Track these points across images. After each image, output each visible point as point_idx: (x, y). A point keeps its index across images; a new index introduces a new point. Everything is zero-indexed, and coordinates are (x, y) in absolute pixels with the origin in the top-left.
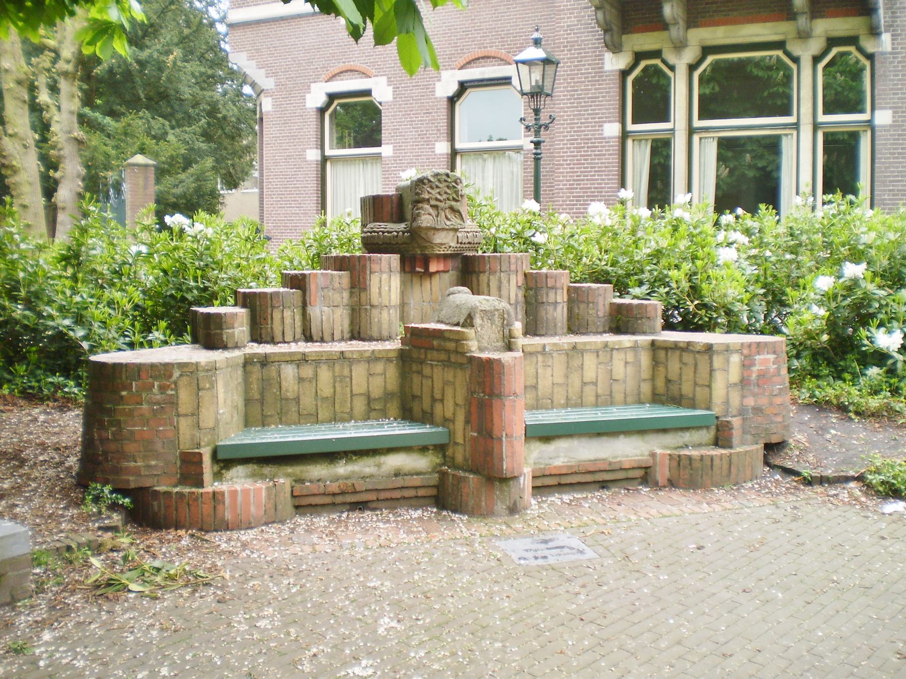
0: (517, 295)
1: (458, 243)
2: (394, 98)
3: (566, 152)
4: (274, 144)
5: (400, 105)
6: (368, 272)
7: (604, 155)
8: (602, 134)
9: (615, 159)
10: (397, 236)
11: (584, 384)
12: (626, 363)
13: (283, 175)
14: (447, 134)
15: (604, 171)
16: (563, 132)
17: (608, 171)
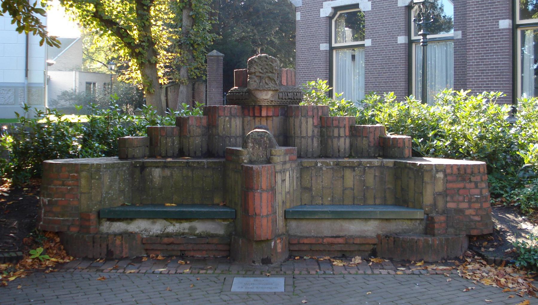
0: (313, 131)
1: (279, 98)
2: (372, 9)
3: (474, 40)
4: (302, 41)
5: (375, 13)
6: (217, 117)
7: (499, 41)
8: (498, 27)
9: (508, 45)
10: (242, 95)
11: (344, 189)
12: (375, 176)
13: (306, 60)
14: (405, 30)
15: (500, 53)
16: (472, 27)
17: (502, 52)
